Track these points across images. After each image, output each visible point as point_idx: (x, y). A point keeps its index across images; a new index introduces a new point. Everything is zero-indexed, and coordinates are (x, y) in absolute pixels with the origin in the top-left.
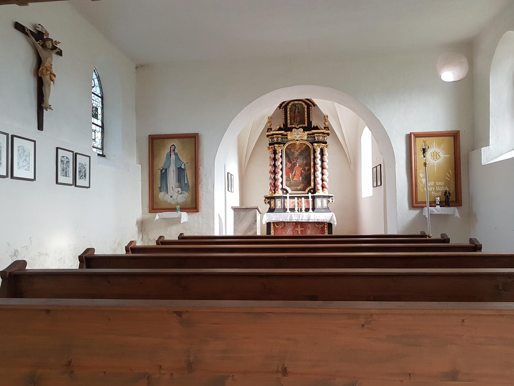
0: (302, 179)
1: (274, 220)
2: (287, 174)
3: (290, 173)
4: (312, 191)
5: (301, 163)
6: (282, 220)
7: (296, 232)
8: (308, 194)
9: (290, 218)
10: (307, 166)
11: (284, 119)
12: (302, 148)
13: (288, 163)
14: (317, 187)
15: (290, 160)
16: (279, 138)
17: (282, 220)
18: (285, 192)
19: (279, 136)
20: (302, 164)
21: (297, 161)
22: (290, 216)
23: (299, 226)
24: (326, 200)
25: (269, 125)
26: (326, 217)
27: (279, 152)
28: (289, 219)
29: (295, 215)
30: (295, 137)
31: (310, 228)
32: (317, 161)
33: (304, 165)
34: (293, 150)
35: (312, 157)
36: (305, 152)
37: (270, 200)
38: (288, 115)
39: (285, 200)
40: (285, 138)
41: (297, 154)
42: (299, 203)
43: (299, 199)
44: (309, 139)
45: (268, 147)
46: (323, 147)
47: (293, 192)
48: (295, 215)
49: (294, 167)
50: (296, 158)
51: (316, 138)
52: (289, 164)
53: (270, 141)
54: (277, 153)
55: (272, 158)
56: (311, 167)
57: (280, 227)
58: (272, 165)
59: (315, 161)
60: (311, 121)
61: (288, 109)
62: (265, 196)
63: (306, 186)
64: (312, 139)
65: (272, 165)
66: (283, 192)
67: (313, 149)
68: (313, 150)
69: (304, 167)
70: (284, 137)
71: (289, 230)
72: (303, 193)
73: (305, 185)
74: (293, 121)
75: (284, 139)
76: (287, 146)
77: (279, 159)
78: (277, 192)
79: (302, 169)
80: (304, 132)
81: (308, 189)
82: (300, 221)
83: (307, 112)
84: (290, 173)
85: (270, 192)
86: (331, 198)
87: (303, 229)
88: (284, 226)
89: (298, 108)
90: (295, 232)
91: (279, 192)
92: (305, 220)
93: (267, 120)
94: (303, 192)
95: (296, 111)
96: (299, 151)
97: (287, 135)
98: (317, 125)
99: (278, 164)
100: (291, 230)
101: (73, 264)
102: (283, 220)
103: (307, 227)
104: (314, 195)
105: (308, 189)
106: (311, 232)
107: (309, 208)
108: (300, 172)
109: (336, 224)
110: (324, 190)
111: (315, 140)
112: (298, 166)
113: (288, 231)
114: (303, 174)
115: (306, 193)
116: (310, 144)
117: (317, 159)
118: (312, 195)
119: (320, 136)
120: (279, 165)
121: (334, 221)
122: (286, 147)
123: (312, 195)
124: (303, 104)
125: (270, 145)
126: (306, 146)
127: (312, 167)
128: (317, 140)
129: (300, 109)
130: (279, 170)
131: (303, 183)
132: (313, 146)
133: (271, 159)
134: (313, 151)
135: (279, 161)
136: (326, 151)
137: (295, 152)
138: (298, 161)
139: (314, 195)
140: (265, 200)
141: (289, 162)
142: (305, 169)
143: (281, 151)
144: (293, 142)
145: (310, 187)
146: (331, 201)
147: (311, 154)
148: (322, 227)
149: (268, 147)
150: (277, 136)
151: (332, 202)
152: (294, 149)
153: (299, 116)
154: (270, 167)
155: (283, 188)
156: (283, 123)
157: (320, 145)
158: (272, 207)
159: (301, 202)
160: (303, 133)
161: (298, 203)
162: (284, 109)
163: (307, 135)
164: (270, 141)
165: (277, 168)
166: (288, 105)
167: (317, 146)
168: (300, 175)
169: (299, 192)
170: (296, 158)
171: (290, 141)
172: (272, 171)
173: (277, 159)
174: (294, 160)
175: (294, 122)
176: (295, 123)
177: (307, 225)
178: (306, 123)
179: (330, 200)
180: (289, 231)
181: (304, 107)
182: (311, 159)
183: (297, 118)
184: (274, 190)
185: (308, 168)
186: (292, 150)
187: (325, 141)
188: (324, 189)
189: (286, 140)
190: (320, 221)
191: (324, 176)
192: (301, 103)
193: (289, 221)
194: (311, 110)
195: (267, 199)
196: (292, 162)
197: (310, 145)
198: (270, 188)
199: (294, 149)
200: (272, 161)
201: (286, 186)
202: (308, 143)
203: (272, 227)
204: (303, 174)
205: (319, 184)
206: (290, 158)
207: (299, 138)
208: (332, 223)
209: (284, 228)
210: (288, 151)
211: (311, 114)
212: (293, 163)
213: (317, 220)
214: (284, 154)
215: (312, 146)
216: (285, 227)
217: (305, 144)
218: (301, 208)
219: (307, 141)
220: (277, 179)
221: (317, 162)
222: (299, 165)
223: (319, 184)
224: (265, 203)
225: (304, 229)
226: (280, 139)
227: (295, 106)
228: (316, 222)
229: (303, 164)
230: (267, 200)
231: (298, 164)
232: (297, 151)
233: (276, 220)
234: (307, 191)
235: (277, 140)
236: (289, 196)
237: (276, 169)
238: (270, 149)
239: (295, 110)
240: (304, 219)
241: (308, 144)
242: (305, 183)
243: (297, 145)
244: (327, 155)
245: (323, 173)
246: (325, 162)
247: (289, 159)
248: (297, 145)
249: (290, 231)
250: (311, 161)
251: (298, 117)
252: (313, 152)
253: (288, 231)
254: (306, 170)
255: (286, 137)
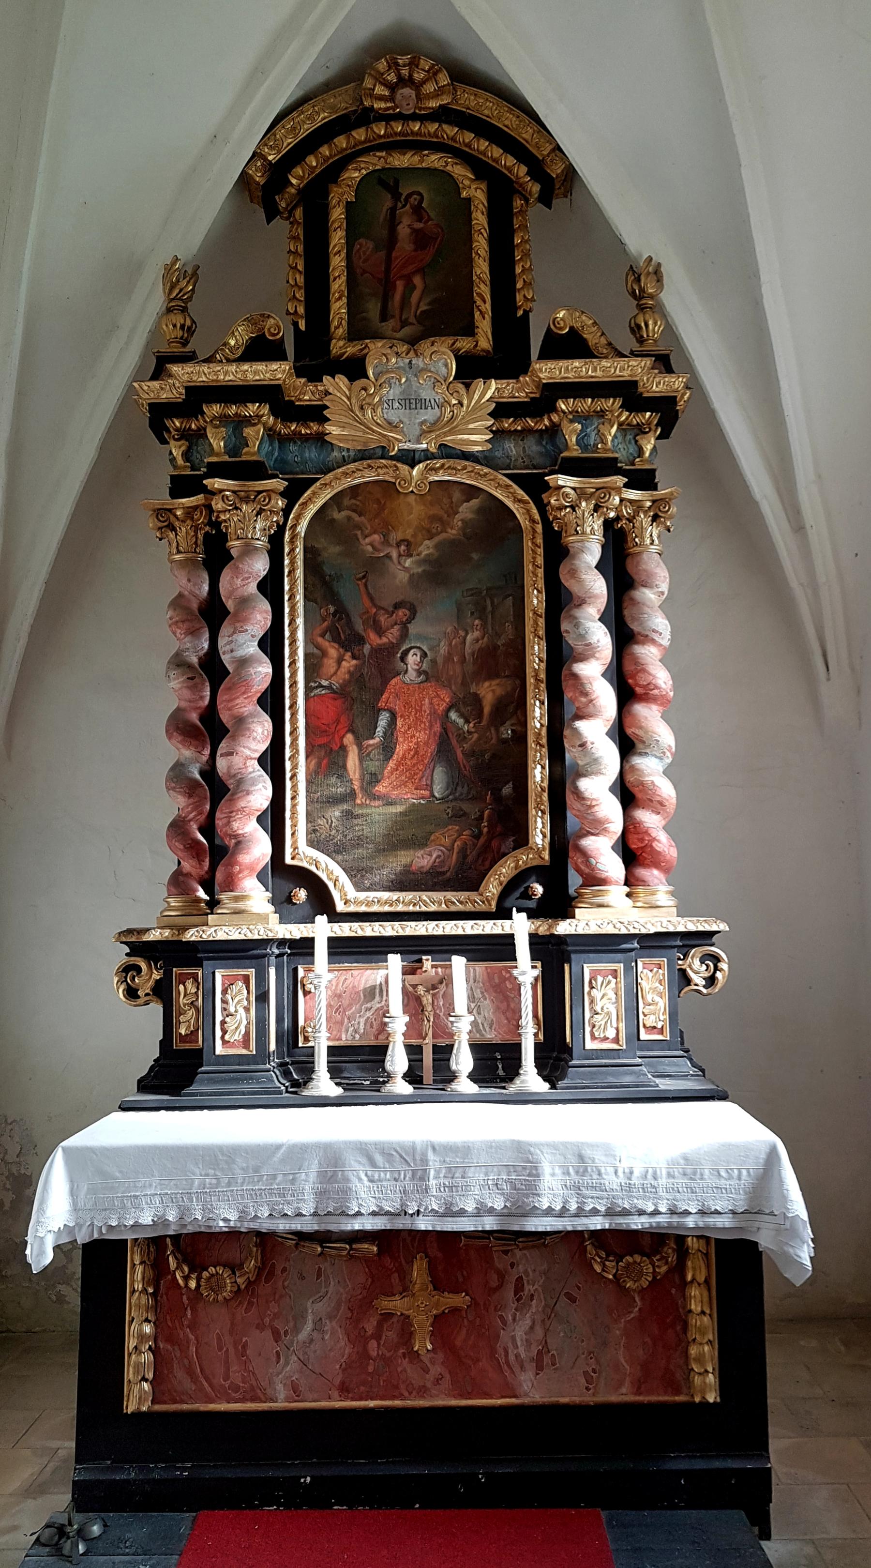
0: (453, 784)
1: (147, 1219)
2: (323, 740)
3: (353, 732)
4: (539, 889)
5: (443, 649)
6: (233, 1216)
7: (391, 1335)
8: (503, 913)
9: (321, 1195)
10: (497, 676)
11: (300, 295)
12: (445, 525)
13: (333, 652)
14: (585, 855)
15: (349, 622)
16: (248, 431)
17: (233, 1216)
18: (302, 894)
19: (252, 409)
20: (448, 658)
21: (404, 635)
22: (322, 1174)
23: (418, 1271)
24: (664, 972)
25: (170, 331)
26: (696, 1184)
27: (249, 550)
28: (307, 1208)
29: (373, 1163)
30: (392, 426)
31: (528, 1288)
32: (577, 625)
33: (470, 667)
34: (376, 537)
35: (536, 600)
36: (475, 556)
37: (168, 975)
38: (337, 262)
39: (301, 973)
40: (306, 438)
41: (402, 577)
42: (427, 1000)
43: (428, 962)
44: (511, 447)
45: (159, 512)
46: (626, 511)
47: (372, 895)
48: (373, 1163)
49: (385, 682)
50: (397, 606)
51: (571, 432)
52: (340, 661)
53: (180, 461)
54: (232, 558)
55: (195, 606)
56: (530, 680)
57: (216, 1284)
58: (194, 660)
59: (565, 626)
60: (526, 313)
61: (337, 214)
62: (130, 931)
63: (482, 840)
64: (532, 446)
65: (190, 666)
66: (289, 900)
67: (539, 528)
68: (540, 540)
69: (464, 684)
70: (297, 434)
71: (314, 1309)
72: (460, 907)
73: (477, 837)
74: (373, 309)
75: (292, 447)
76: (320, 503)
77: (244, 602)
78: (223, 897)
79: (446, 697)
80: (467, 386)
81: (505, 870)
82: (423, 1224)
83: (491, 241)
84: (349, 739)
85: (174, 902)
86: (696, 953)
87: (460, 1300)
88: (266, 1271)
89: (418, 211)
90: (377, 1336)
91: (240, 905)
92: (482, 1211)
93: (158, 300)
94: (456, 899)
95: (403, 231)
96: (427, 548)
97: (317, 413)
98: (577, 325)
99: (240, 653)
100: (331, 1318)
101: (277, 915)
102: (243, 1213)
103: (502, 1276)
104: (564, 928)
105: (505, 870)
106: (539, 1332)
107: (510, 1039)
108: (437, 728)
109: (805, 1254)
110: (643, 883)
111: (567, 447)
112: (419, 672)
113: (309, 1326)
114: (454, 742)
115: (483, 908)
116: (521, 493)
117: (578, 613)
118: (542, 927)
119: (601, 414)
120: (244, 662)
121: (789, 1229)
122: (312, 510)
123: (542, 927)
124: (460, 171)
125: (175, 493)
126: (480, 511)
127: (538, 680)
128: (575, 451)
129: (432, 214)
130: (248, 706)
131: (458, 816)
132: (542, 508)
133: (187, 609)
134: (540, 551)
135: (245, 620)
136: (654, 549)
137: (394, 555)
138: (413, 629)
139: (564, 928)
140: (127, 969)
141: (336, 639)
142: (477, 700)
143: (262, 543)
144: (370, 476)
145: (524, 859)
146: (698, 980)
147: (528, 579)
148: (654, 1283)
149: (159, 512)
150: (233, 410)
151: (711, 981)
152: (385, 536)
153: (421, 271)
154: (176, 682)
155: (288, 861)
156: (295, 324)
157: (608, 490)
158: (183, 1039)
159: (442, 988)
160: (460, 387)
161: (418, 999)
162: (299, 213)
163: (492, 414)
164: (173, 460)
165: (229, 689)
166: (335, 181)
167: (581, 493)
168: (433, 747)
169: (424, 896)
170: (397, 606)
171: (344, 462)
172: (194, 717)
173: (230, 605)
174: (383, 619)
175: (384, 316)
176: (391, 323)
177: (500, 1262)
178: (484, 326)
179: (697, 970)
180: (318, 1326)
181: (468, 200)
182: (529, 615)
183: (410, 287)
184: (208, 885)
185: (499, 691)
186: (369, 543)
187: (639, 465)
188: (642, 872)
189: (312, 453)
190: (637, 1223)
191: (638, 761)
192: (439, 165)
193: (308, 1225)
194: (524, 227)
195: (148, 959)
196: (361, 640)
197: (520, 501)
198: (179, 863)
199: (385, 536)
200: (193, 633)
201: (311, 843)
202: (499, 486)
203: (139, 1286)
204: (462, 737)
205: (604, 831)
206: (350, 606)
207: (423, 434)
208: (765, 1240)
209: (264, 1289)
210: (331, 551)
211: (526, 255)
212: (377, 651)
213: (610, 1213)
214: (300, 573)
215: (535, 511)
216: (271, 1274)
217: (471, 492)
218: (442, 1042)
219: (496, 468)
220: (231, 786)
221: (582, 637)
222: (425, 666)
223: (597, 827)
224: (132, 993)
225: (474, 1303)
226: (254, 434)
227: (396, 196)
228: (597, 1235)
229: (463, 659)
230: (144, 966)
231: (412, 659)
232: (409, 546)
233: (172, 1216)
234: (492, 888)
235: (233, 451)
236: (331, 940)
237: (221, 697)
238: (173, 529)
239: (392, 222)
240: (470, 1207)
241: (498, 494)
242: (481, 818)
243: (411, 499)
244: (664, 587)
245: (629, 731)
246: (646, 639)
247: (341, 612)
248: (411, 499)
249: (328, 1326)
250: (529, 628)
251: (417, 280)
252: (540, 561)
253: (309, 1326)
254: (487, 710)
255: (315, 427)
